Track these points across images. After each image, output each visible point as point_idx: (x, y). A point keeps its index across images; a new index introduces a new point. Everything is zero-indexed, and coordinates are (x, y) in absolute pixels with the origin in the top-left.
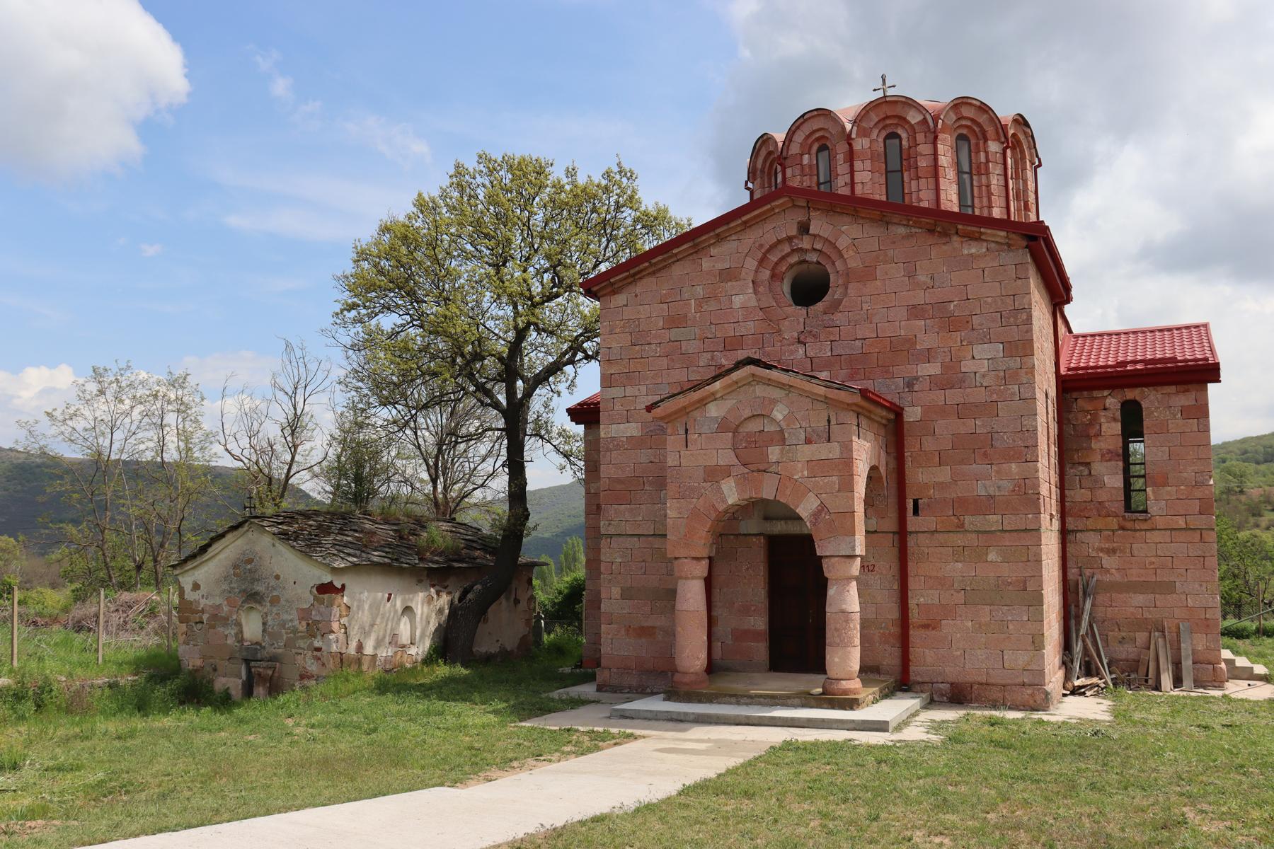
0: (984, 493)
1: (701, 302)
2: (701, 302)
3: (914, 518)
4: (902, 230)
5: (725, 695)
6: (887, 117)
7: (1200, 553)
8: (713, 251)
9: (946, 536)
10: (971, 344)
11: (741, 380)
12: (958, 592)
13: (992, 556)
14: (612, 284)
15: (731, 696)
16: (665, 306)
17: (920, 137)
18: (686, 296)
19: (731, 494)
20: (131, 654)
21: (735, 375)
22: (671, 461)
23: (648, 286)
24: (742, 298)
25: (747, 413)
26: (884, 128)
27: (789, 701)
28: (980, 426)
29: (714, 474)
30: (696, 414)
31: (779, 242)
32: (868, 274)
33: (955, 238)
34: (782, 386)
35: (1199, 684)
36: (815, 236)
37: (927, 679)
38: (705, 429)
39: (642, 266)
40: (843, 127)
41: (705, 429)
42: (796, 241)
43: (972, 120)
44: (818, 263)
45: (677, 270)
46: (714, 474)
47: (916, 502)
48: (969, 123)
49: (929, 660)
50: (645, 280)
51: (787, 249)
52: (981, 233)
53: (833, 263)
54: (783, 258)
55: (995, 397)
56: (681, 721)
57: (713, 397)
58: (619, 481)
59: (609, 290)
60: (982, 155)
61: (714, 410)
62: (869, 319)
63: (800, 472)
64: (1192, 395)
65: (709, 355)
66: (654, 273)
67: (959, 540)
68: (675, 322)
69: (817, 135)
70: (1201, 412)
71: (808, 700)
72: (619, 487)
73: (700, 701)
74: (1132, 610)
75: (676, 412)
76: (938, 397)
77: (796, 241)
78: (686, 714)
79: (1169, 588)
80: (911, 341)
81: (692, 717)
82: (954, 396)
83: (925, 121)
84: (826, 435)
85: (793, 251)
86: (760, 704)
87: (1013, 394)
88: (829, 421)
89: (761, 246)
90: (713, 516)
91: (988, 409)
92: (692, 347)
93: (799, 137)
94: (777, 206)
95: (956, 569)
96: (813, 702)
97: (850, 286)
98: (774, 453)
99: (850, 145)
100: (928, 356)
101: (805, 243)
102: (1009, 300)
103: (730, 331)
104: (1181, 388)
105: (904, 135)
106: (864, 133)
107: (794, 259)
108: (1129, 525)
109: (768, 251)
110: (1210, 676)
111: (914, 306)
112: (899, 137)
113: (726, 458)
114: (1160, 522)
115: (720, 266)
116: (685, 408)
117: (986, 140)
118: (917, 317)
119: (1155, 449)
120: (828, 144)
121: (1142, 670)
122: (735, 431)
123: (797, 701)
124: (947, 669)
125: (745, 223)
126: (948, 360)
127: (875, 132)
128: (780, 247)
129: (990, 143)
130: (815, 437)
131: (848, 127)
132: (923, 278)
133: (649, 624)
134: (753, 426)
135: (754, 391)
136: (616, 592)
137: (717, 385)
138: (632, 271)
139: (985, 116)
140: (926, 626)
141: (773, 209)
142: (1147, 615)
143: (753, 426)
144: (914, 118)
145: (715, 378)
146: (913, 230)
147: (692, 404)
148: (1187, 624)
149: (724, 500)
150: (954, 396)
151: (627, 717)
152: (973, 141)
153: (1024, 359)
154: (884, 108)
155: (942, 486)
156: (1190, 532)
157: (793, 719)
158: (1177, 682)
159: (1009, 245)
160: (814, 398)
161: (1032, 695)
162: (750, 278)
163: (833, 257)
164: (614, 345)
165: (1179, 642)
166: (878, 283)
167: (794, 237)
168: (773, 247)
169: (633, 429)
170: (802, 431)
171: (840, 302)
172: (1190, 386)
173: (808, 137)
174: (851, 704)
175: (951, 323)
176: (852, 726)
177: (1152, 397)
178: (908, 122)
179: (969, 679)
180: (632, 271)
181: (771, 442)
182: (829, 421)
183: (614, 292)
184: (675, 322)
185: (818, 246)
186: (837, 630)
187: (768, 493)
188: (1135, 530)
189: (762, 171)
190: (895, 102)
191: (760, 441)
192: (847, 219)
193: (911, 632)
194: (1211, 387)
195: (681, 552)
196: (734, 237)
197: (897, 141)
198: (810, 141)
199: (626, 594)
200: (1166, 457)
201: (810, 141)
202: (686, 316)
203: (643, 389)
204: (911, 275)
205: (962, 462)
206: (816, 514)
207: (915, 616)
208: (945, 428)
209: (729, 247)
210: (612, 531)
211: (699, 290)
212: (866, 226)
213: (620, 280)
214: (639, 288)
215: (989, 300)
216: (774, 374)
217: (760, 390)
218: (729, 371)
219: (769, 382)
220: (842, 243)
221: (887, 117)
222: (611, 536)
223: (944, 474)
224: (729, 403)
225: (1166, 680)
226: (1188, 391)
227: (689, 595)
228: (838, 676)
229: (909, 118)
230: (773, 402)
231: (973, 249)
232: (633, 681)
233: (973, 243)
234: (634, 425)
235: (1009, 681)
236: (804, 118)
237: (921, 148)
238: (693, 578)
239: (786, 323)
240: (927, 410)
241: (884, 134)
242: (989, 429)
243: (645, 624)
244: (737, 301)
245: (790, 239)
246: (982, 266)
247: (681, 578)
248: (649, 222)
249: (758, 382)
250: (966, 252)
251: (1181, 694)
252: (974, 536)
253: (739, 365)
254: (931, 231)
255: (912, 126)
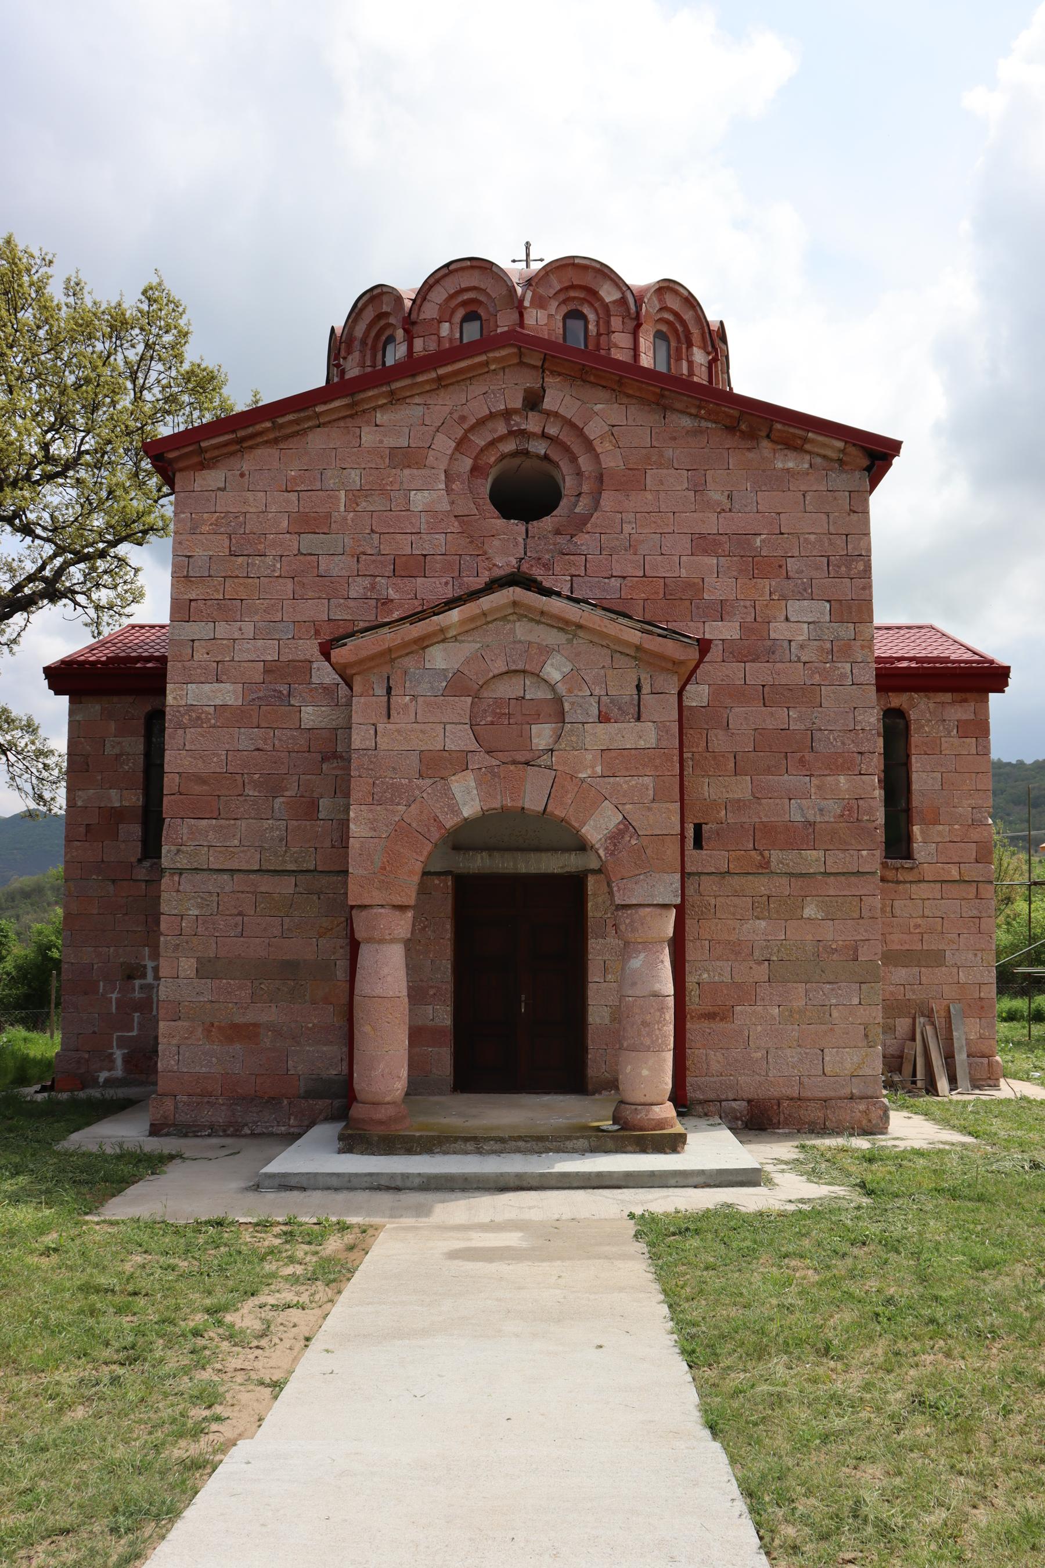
0: (799, 818)
1: (355, 496)
2: (355, 496)
3: (695, 852)
4: (686, 422)
5: (456, 1139)
6: (572, 287)
7: (975, 913)
8: (380, 417)
9: (743, 880)
10: (784, 598)
11: (493, 610)
12: (759, 963)
13: (810, 911)
14: (318, 415)
15: (466, 1139)
16: (293, 496)
17: (616, 322)
18: (331, 483)
19: (468, 797)
20: (446, 1250)
21: (487, 602)
22: (359, 739)
23: (260, 461)
24: (426, 496)
25: (499, 666)
26: (564, 302)
27: (569, 1144)
28: (795, 719)
29: (437, 765)
30: (409, 662)
31: (492, 416)
32: (632, 480)
33: (765, 443)
34: (563, 625)
35: (976, 1084)
36: (548, 414)
37: (712, 1096)
38: (423, 688)
39: (259, 427)
40: (512, 290)
41: (423, 688)
42: (516, 418)
43: (676, 314)
44: (546, 457)
45: (317, 441)
46: (437, 765)
47: (698, 828)
48: (671, 318)
49: (715, 1067)
50: (259, 452)
51: (502, 429)
52: (805, 440)
53: (574, 459)
54: (492, 443)
55: (817, 679)
56: (398, 1189)
57: (441, 636)
58: (200, 780)
59: (195, 460)
60: (685, 364)
61: (439, 658)
62: (631, 547)
63: (590, 768)
64: (971, 706)
65: (367, 582)
66: (276, 441)
67: (762, 885)
68: (308, 523)
69: (466, 296)
70: (980, 729)
71: (600, 1142)
72: (198, 789)
73: (409, 1151)
74: (892, 988)
75: (372, 658)
76: (734, 672)
77: (516, 418)
78: (405, 1176)
79: (936, 959)
80: (694, 588)
81: (417, 1181)
82: (758, 673)
83: (623, 301)
84: (633, 710)
85: (511, 433)
86: (518, 1151)
87: (843, 676)
88: (639, 687)
89: (463, 418)
90: (436, 835)
91: (806, 695)
92: (337, 566)
93: (439, 295)
94: (495, 360)
95: (757, 929)
96: (610, 1144)
97: (605, 495)
98: (542, 735)
99: (521, 315)
100: (721, 611)
101: (532, 423)
102: (840, 541)
103: (404, 546)
104: (958, 696)
105: (591, 317)
106: (540, 302)
107: (509, 447)
108: (890, 874)
109: (472, 428)
110: (986, 1077)
111: (702, 536)
112: (584, 317)
113: (460, 739)
114: (928, 872)
115: (390, 442)
116: (390, 650)
117: (690, 345)
118: (706, 552)
119: (924, 775)
120: (481, 312)
121: (907, 1069)
122: (476, 697)
123: (582, 1143)
124: (742, 1079)
125: (440, 378)
126: (750, 618)
127: (554, 304)
128: (490, 425)
129: (695, 349)
130: (615, 713)
131: (519, 290)
132: (716, 496)
133: (250, 1017)
134: (508, 689)
135: (513, 631)
136: (187, 966)
137: (455, 615)
138: (241, 433)
139: (691, 313)
140: (711, 1016)
141: (487, 363)
142: (910, 995)
143: (508, 689)
144: (609, 294)
145: (451, 604)
146: (704, 424)
147: (405, 645)
148: (958, 1006)
149: (455, 810)
150: (758, 673)
151: (292, 1188)
152: (673, 344)
153: (861, 627)
154: (570, 272)
155: (739, 805)
156: (963, 886)
157: (599, 1175)
158: (953, 1081)
159: (841, 462)
160: (616, 648)
161: (866, 1113)
162: (443, 467)
163: (576, 448)
164: (198, 552)
165: (950, 1030)
166: (649, 496)
167: (516, 411)
168: (481, 422)
169: (228, 694)
170: (593, 701)
171: (585, 519)
172: (968, 695)
173: (451, 297)
174: (674, 1144)
175: (757, 566)
176: (700, 1180)
177: (922, 706)
178: (601, 299)
179: (775, 1092)
180: (241, 433)
181: (537, 718)
182: (639, 687)
183: (202, 466)
184: (308, 523)
185: (552, 430)
186: (645, 1024)
187: (533, 800)
188: (898, 882)
189: (364, 342)
190: (585, 268)
191: (518, 715)
192: (602, 394)
193: (688, 1025)
194: (992, 696)
195: (376, 897)
196: (417, 400)
197: (581, 323)
198: (453, 303)
199: (206, 969)
200: (938, 787)
201: (453, 303)
202: (329, 515)
203: (249, 629)
204: (698, 489)
205: (768, 771)
206: (615, 838)
207: (694, 1002)
208: (745, 718)
209: (410, 413)
210: (182, 862)
211: (354, 477)
212: (632, 409)
213: (291, 422)
214: (248, 463)
215: (812, 537)
216: (555, 605)
217: (522, 631)
218: (474, 595)
219: (542, 617)
220: (594, 430)
221: (572, 287)
222: (181, 872)
223: (741, 788)
224: (468, 648)
225: (943, 1084)
226: (965, 701)
227: (386, 970)
228: (648, 1099)
229: (602, 293)
230: (547, 651)
231: (790, 462)
232: (221, 1117)
233: (791, 454)
234: (228, 686)
235: (832, 1094)
236: (449, 270)
237: (617, 338)
238: (393, 941)
239: (496, 543)
240: (718, 691)
241: (564, 309)
242: (809, 725)
243: (239, 1020)
244: (419, 500)
245: (507, 414)
246: (803, 488)
247: (370, 940)
248: (202, 382)
249: (521, 617)
250: (779, 465)
251: (959, 1097)
252: (785, 880)
253: (494, 585)
254: (731, 429)
255: (606, 307)
